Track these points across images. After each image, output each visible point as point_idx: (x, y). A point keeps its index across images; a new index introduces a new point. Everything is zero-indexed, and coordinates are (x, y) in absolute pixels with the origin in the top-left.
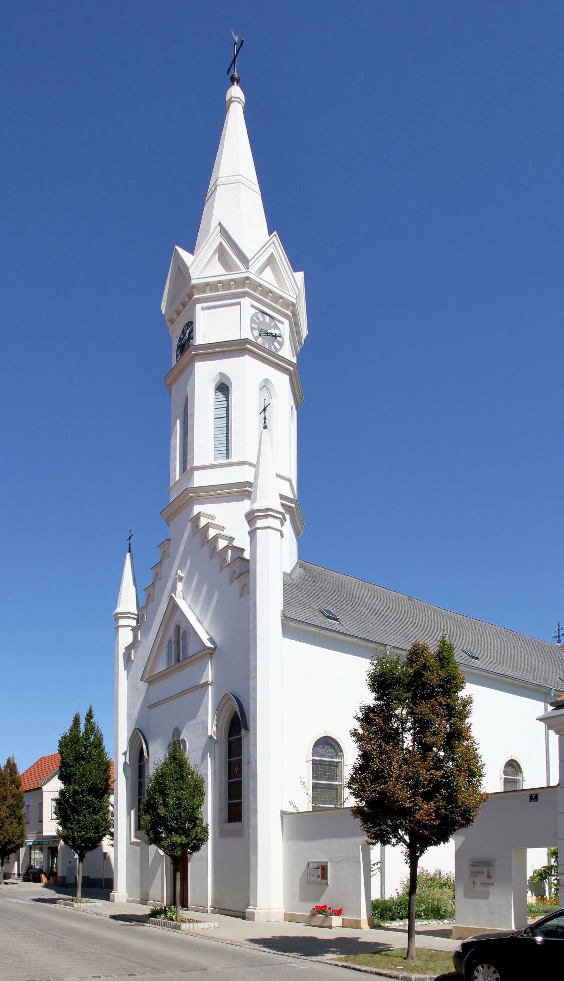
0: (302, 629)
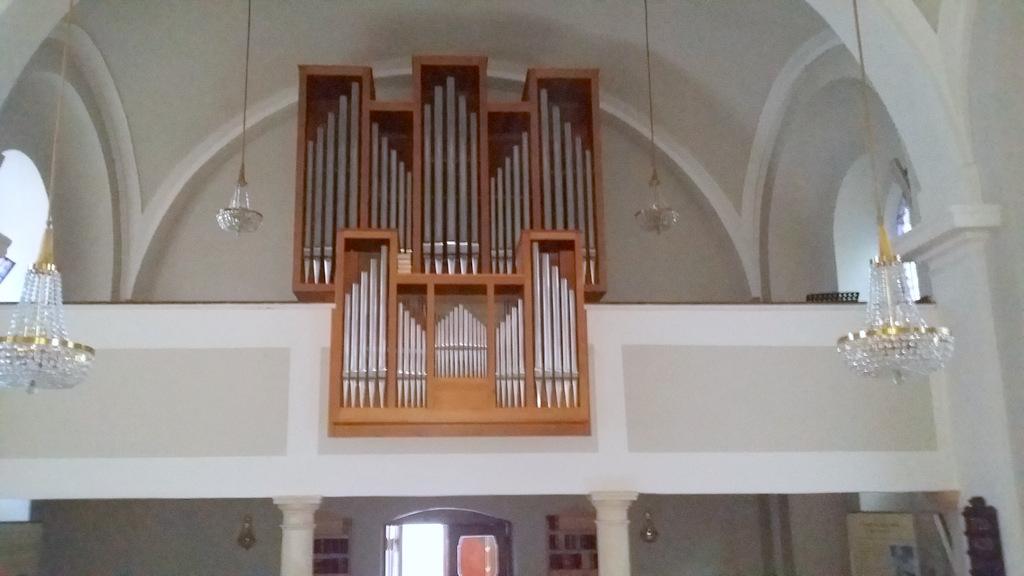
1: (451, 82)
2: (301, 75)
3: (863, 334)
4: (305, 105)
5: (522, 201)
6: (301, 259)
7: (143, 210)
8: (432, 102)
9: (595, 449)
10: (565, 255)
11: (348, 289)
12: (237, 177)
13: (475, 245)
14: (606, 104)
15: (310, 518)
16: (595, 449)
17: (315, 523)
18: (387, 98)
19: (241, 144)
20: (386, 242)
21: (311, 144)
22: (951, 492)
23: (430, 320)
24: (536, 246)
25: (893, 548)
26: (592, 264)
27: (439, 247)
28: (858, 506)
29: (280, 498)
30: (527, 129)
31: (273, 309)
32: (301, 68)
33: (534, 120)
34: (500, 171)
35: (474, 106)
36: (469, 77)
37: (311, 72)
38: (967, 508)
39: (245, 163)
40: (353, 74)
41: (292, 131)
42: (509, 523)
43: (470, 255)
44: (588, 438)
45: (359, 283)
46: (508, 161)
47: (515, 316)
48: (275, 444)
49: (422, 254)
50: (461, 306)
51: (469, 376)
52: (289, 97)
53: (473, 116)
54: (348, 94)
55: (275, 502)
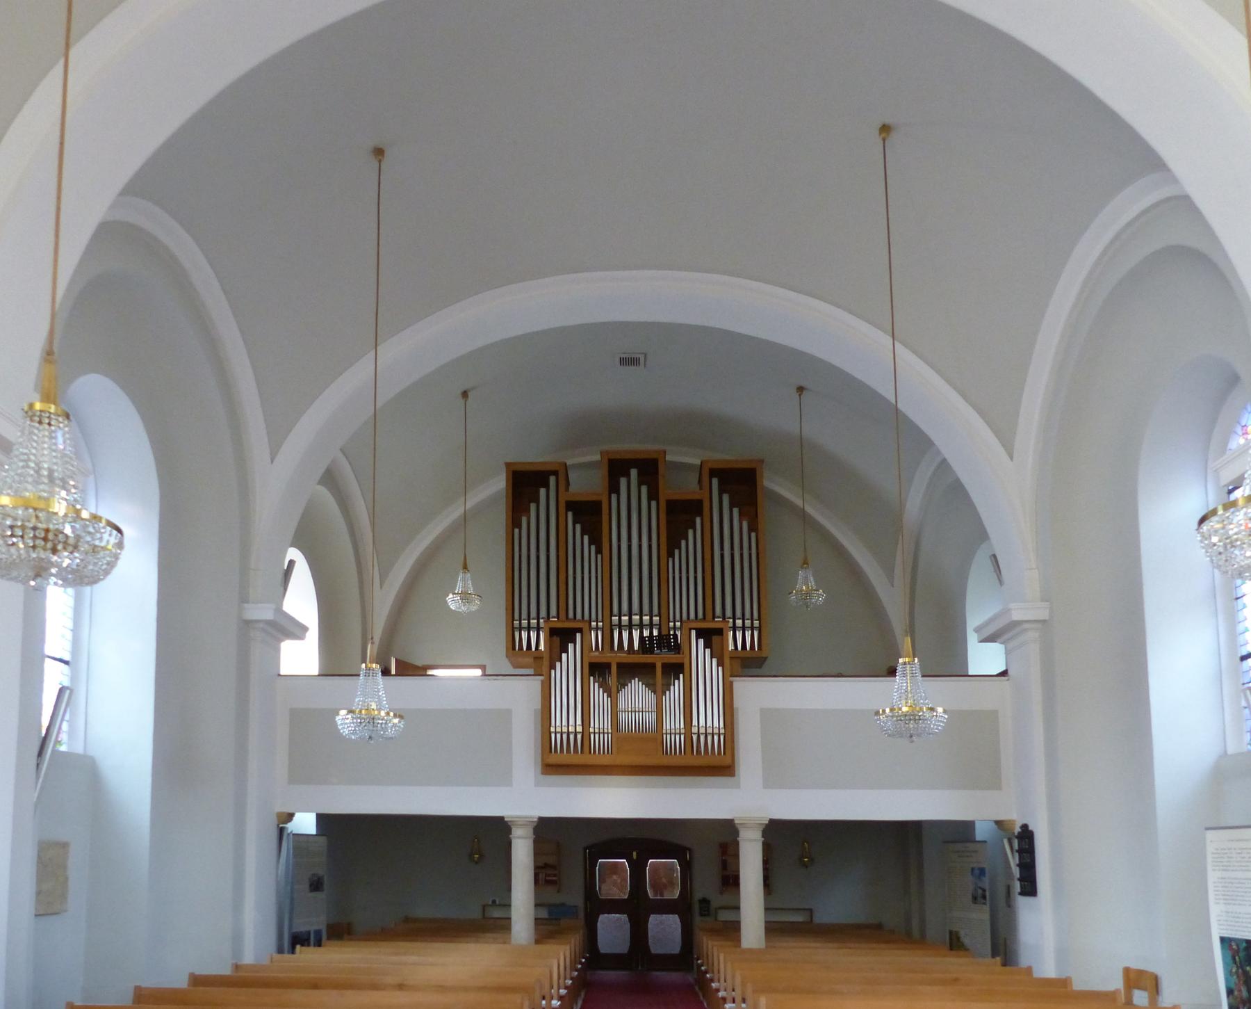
1: (634, 473)
3: (888, 710)
4: (510, 491)
5: (696, 578)
6: (512, 630)
7: (381, 588)
8: (617, 492)
9: (738, 786)
10: (715, 639)
11: (553, 667)
13: (656, 619)
15: (531, 831)
16: (738, 786)
17: (534, 834)
19: (465, 517)
20: (580, 630)
21: (516, 531)
22: (1010, 821)
23: (614, 690)
24: (693, 633)
25: (973, 869)
26: (756, 633)
27: (625, 620)
28: (975, 838)
29: (508, 817)
30: (700, 514)
32: (508, 465)
33: (706, 505)
34: (677, 552)
35: (653, 495)
36: (649, 469)
38: (1019, 833)
39: (467, 553)
40: (548, 468)
41: (500, 516)
42: (690, 850)
44: (732, 779)
45: (561, 661)
46: (683, 543)
47: (677, 688)
48: (503, 777)
49: (611, 625)
50: (637, 679)
51: (628, 731)
52: (498, 484)
53: (654, 503)
54: (547, 486)
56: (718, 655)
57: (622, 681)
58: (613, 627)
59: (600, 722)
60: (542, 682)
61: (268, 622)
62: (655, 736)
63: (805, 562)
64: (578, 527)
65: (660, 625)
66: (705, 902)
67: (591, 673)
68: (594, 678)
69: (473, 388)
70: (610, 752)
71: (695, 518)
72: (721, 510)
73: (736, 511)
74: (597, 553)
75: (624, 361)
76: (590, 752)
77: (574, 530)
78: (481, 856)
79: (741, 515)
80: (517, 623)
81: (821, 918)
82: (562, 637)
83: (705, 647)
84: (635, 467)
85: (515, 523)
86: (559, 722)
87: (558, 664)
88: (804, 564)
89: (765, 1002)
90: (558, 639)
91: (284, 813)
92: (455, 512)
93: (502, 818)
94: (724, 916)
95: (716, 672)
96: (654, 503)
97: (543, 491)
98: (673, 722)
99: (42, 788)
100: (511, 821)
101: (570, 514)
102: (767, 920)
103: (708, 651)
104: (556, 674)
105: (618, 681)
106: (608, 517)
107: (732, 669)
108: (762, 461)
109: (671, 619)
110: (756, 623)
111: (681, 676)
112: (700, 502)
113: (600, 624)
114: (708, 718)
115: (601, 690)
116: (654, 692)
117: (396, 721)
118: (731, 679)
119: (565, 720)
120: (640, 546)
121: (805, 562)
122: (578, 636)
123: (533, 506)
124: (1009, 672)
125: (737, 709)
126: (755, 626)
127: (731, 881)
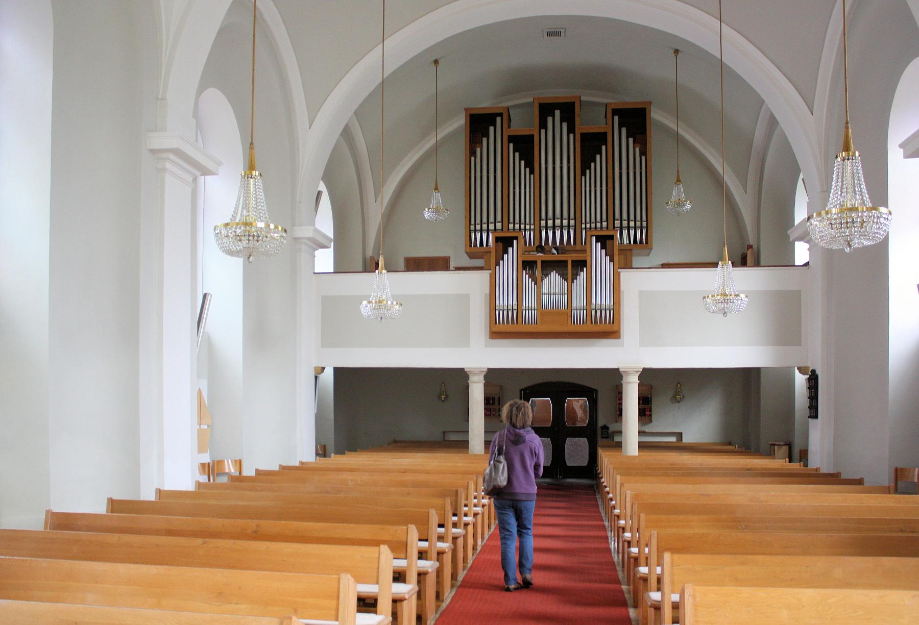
0: (172, 515)
1: (557, 113)
2: (466, 115)
9: (623, 345)
11: (497, 264)
12: (433, 186)
14: (656, 115)
16: (623, 345)
18: (519, 127)
19: (436, 148)
20: (516, 238)
21: (473, 158)
23: (539, 279)
29: (467, 368)
31: (460, 273)
32: (466, 110)
34: (588, 171)
35: (571, 130)
36: (568, 111)
37: (473, 112)
41: (462, 143)
43: (569, 226)
46: (593, 165)
47: (582, 276)
49: (540, 227)
51: (548, 308)
52: (460, 122)
53: (571, 136)
55: (465, 370)
56: (610, 254)
57: (545, 272)
58: (542, 228)
59: (529, 301)
60: (490, 274)
61: (310, 239)
62: (565, 312)
63: (678, 181)
64: (517, 154)
65: (575, 226)
66: (605, 428)
67: (524, 268)
68: (526, 271)
69: (441, 58)
70: (536, 323)
71: (601, 146)
72: (620, 139)
73: (631, 140)
74: (530, 173)
75: (549, 34)
76: (522, 323)
77: (514, 157)
78: (447, 396)
79: (634, 142)
80: (472, 227)
81: (687, 439)
82: (505, 243)
83: (602, 248)
84: (558, 109)
85: (473, 153)
86: (501, 302)
87: (501, 262)
88: (677, 181)
89: (619, 479)
90: (502, 244)
91: (319, 367)
92: (430, 143)
93: (463, 369)
94: (617, 439)
95: (609, 266)
96: (571, 136)
97: (492, 129)
98: (579, 301)
99: (199, 350)
100: (470, 371)
101: (511, 145)
102: (640, 441)
103: (604, 251)
104: (500, 270)
105: (542, 273)
106: (538, 146)
107: (619, 264)
108: (651, 103)
109: (583, 221)
110: (644, 224)
111: (585, 269)
112: (605, 134)
113: (532, 227)
114: (602, 298)
115: (530, 279)
116: (566, 280)
117: (397, 307)
118: (619, 270)
119: (507, 300)
120: (561, 168)
121: (678, 181)
122: (515, 242)
123: (485, 140)
124: (810, 263)
125: (623, 291)
126: (643, 226)
127: (619, 413)
